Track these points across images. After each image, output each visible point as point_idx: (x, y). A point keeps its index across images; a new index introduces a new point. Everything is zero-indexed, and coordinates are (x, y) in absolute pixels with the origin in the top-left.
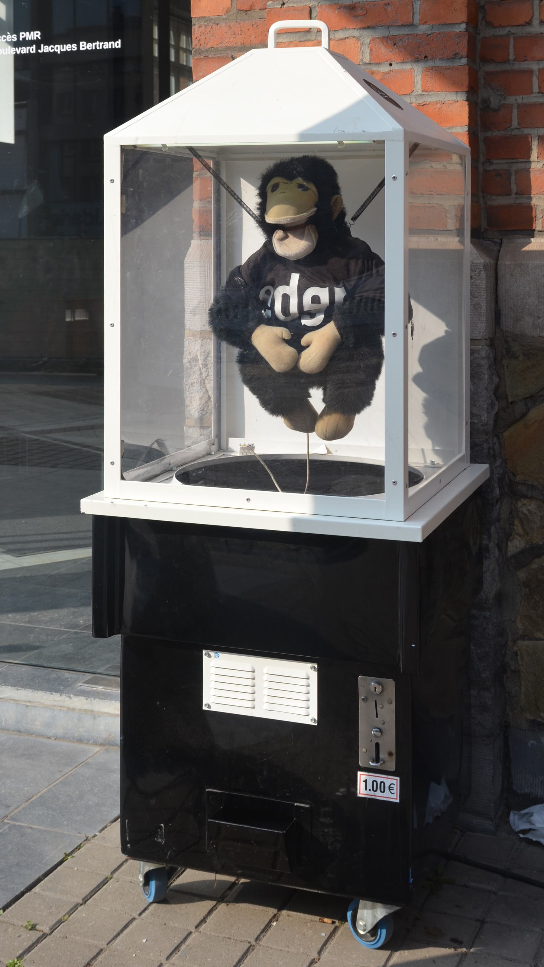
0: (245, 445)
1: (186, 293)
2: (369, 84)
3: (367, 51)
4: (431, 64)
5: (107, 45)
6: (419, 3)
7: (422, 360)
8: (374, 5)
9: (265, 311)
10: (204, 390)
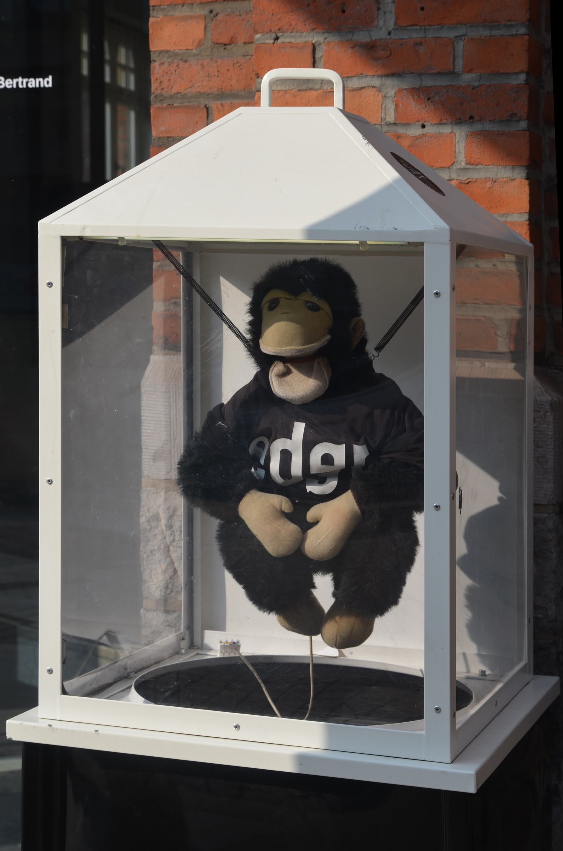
0: (227, 642)
1: (143, 427)
2: (398, 158)
3: (391, 106)
4: (478, 127)
5: (33, 83)
6: (462, 43)
7: (468, 536)
8: (401, 45)
9: (256, 469)
10: (169, 560)
